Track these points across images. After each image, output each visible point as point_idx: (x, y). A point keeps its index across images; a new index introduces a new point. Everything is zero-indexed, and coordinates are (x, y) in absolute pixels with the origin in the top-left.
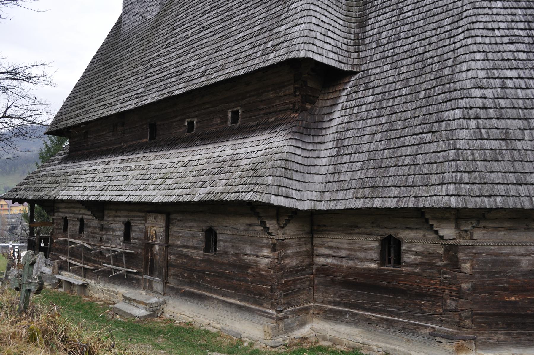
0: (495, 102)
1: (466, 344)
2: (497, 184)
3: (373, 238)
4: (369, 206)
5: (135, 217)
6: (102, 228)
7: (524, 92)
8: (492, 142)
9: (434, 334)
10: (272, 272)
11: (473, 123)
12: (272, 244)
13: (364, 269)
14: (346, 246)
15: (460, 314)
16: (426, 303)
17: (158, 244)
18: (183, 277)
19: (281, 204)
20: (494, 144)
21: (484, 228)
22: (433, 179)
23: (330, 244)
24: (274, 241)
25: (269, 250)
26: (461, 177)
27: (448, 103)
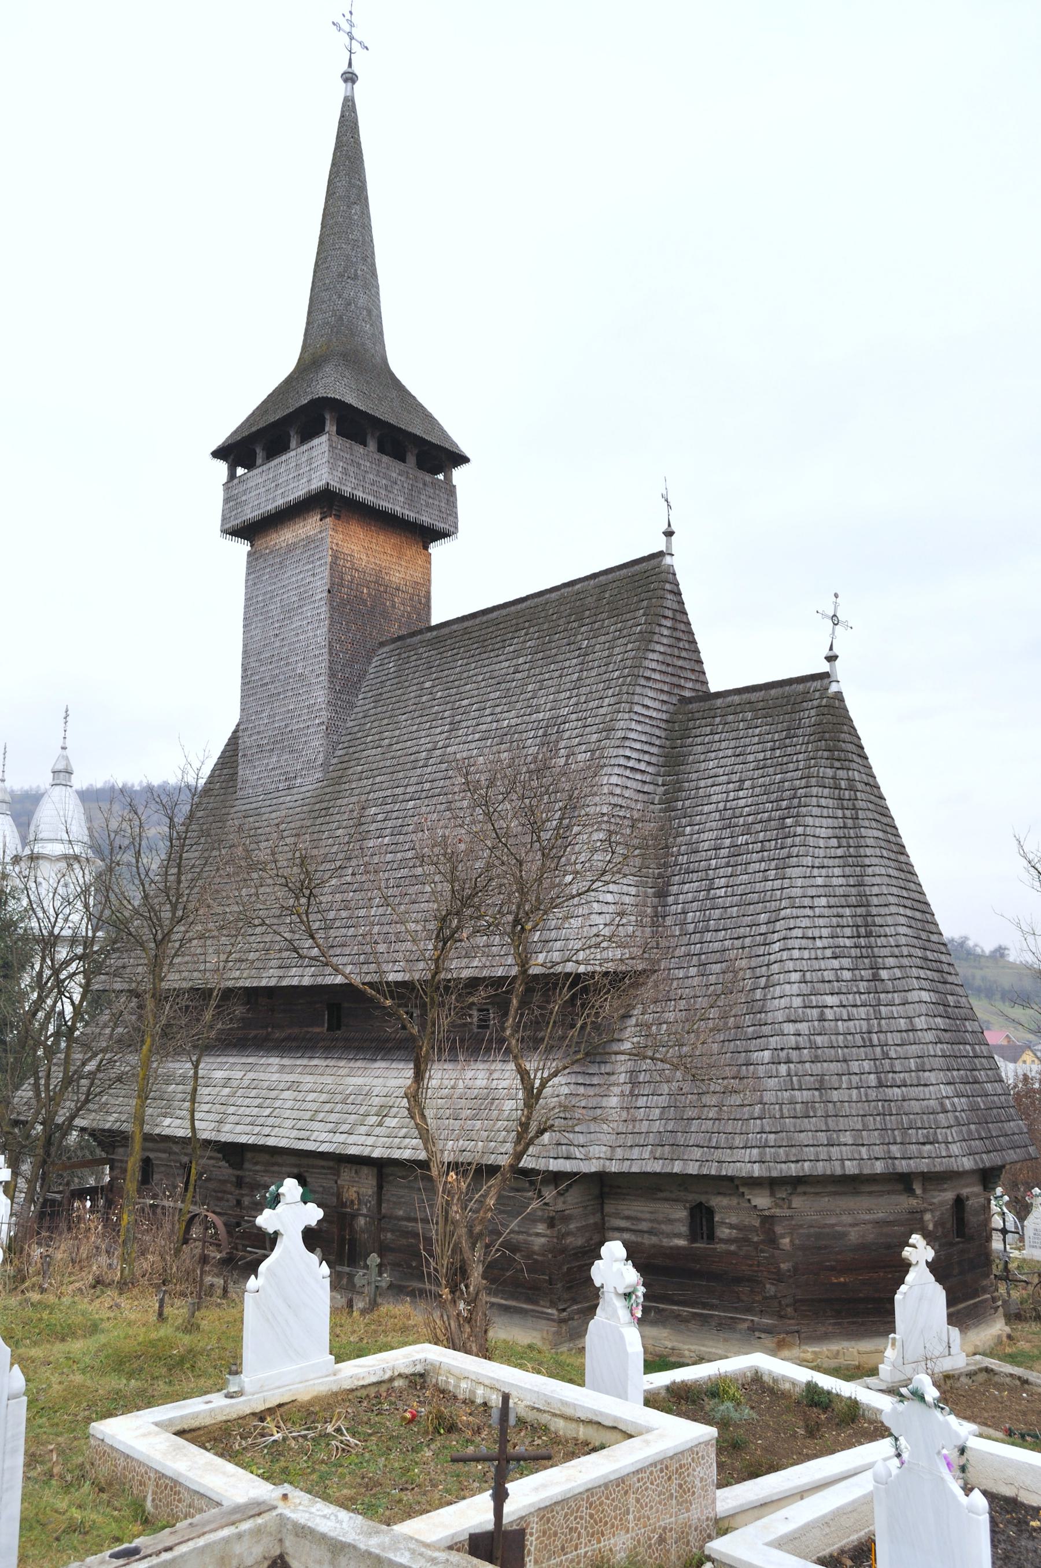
0: (810, 1040)
1: (789, 1338)
2: (806, 1146)
3: (680, 1206)
4: (668, 1170)
5: (314, 1167)
6: (239, 1183)
7: (846, 1024)
8: (805, 1092)
9: (753, 1329)
10: (550, 1256)
11: (783, 1069)
12: (549, 1217)
13: (671, 1248)
14: (648, 1216)
15: (780, 1302)
16: (744, 1289)
17: (362, 1215)
18: (410, 1266)
19: (562, 1169)
20: (806, 1095)
21: (805, 1193)
22: (738, 1141)
23: (627, 1213)
24: (552, 1214)
25: (546, 1225)
26: (766, 1140)
27: (758, 1040)
